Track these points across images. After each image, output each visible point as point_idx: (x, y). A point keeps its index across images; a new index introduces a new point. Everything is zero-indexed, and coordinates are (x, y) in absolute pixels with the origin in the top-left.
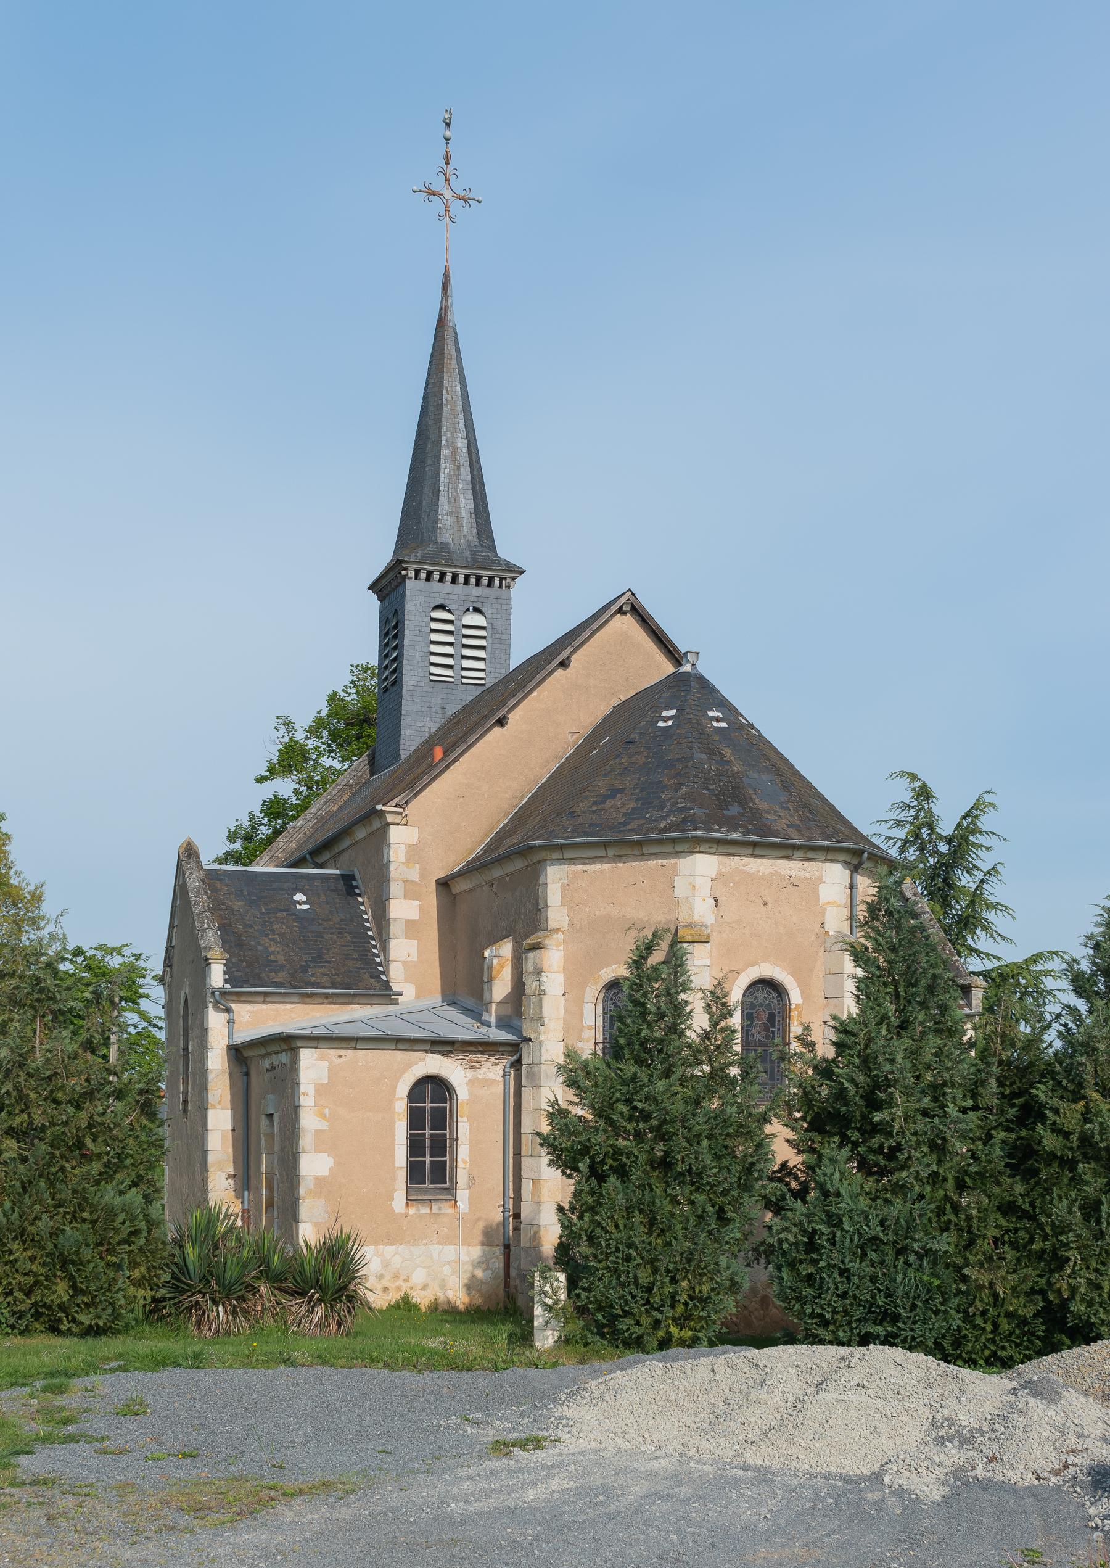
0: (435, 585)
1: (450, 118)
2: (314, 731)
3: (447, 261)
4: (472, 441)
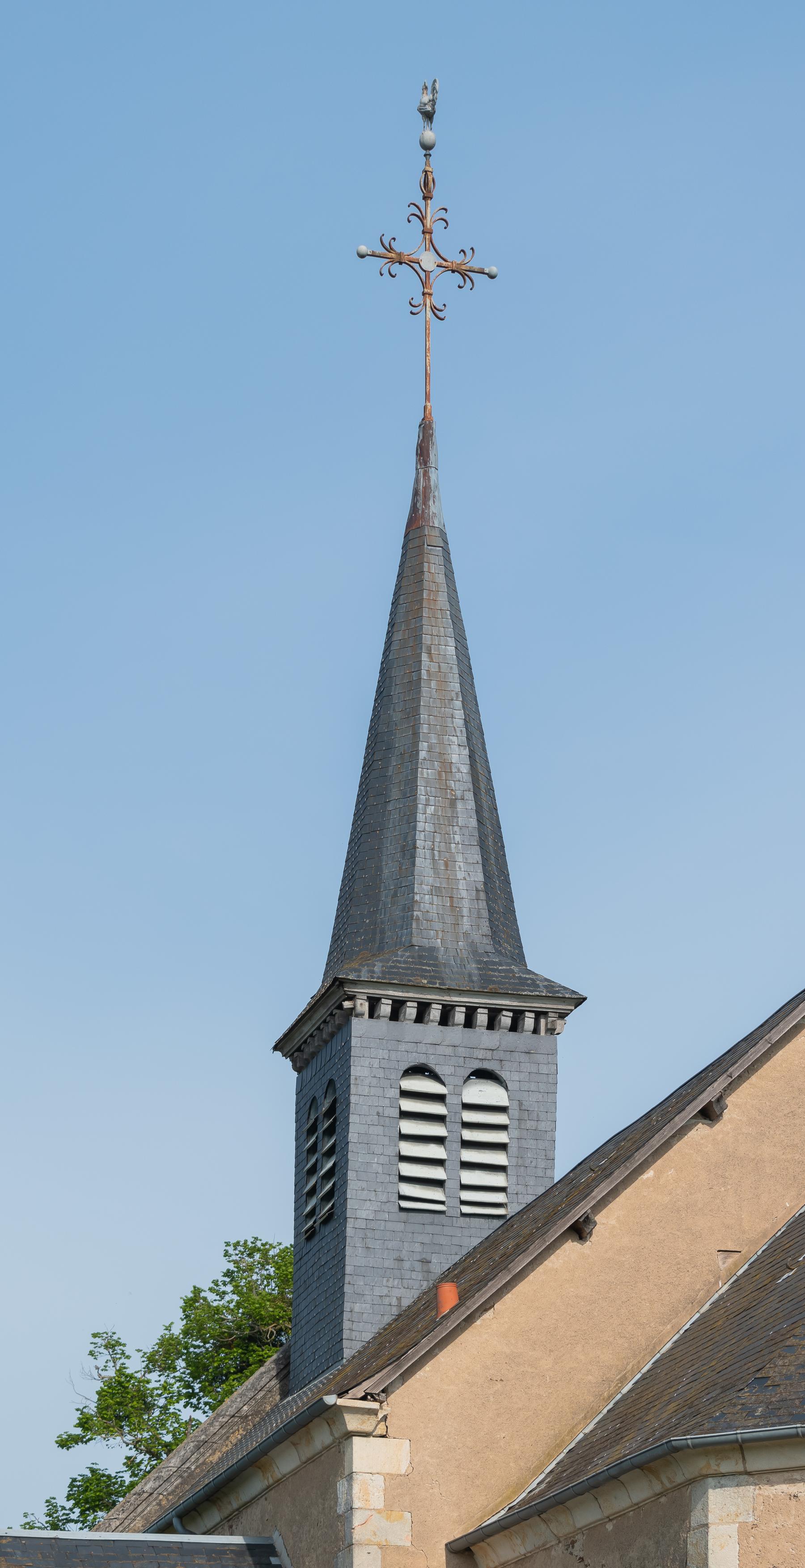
0: (408, 1026)
1: (433, 102)
2: (163, 1356)
3: (427, 397)
4: (479, 752)
